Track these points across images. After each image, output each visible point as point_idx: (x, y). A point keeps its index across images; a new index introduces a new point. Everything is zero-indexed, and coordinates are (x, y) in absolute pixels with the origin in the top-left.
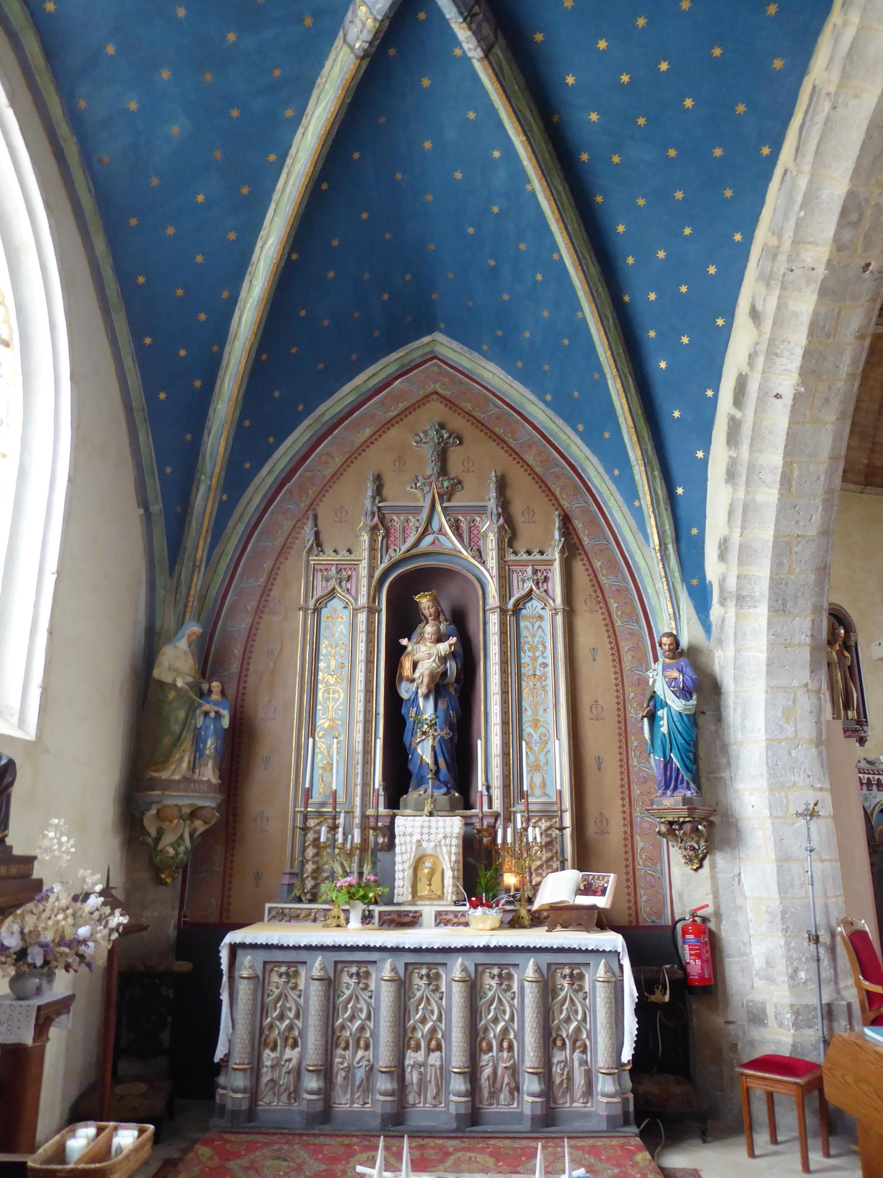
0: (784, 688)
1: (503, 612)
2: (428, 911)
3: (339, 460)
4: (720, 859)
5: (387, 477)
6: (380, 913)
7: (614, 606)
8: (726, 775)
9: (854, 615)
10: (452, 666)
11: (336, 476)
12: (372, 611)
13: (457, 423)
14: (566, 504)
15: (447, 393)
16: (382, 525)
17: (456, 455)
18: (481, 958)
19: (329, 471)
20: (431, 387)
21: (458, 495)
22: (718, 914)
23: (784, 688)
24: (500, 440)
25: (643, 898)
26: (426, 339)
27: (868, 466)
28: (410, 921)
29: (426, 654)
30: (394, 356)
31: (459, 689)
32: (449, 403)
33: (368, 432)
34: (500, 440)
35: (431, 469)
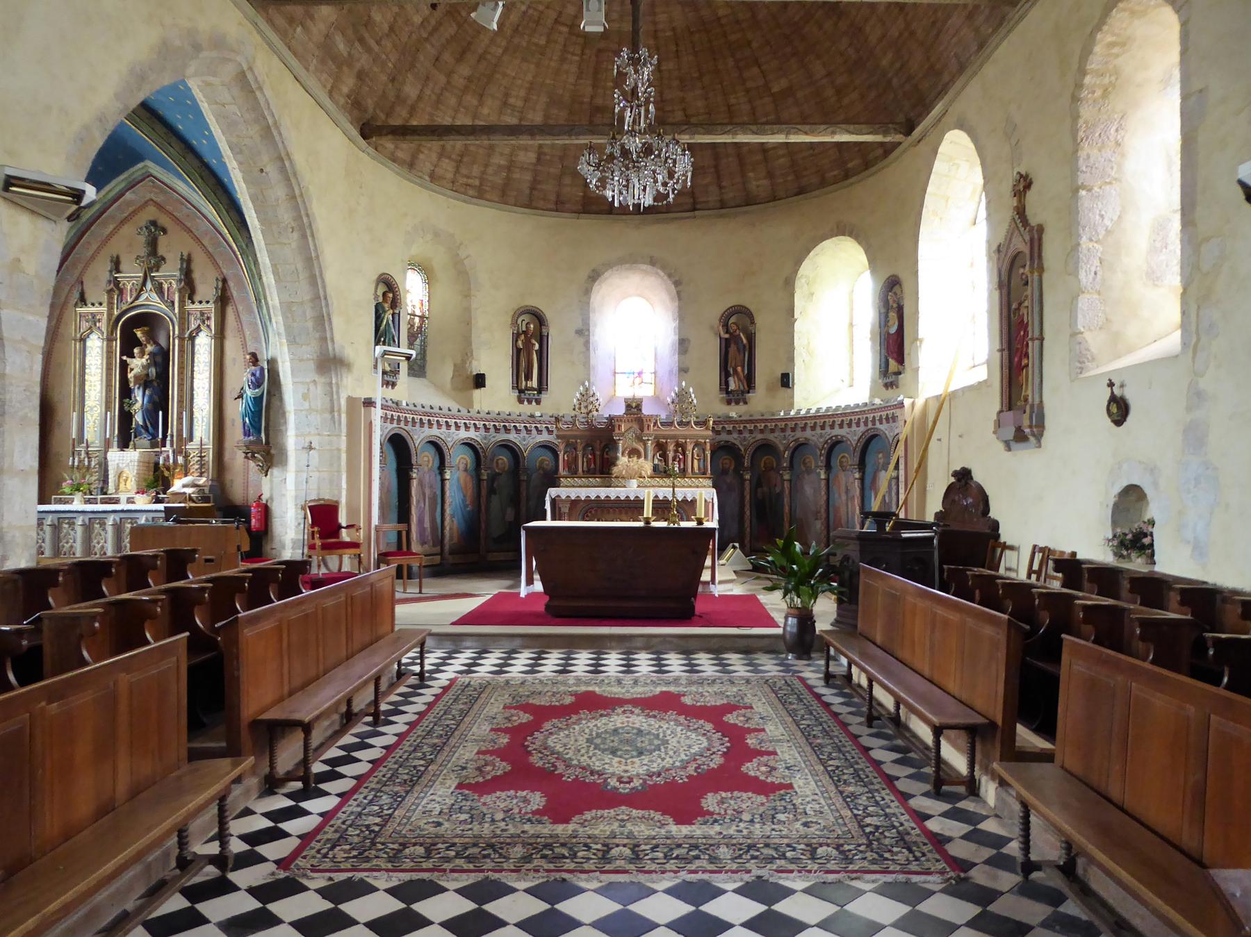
0: (302, 383)
1: (181, 339)
2: (123, 497)
3: (94, 247)
4: (275, 472)
5: (123, 259)
6: (544, 519)
7: (247, 333)
8: (283, 428)
9: (549, 314)
10: (153, 371)
11: (93, 258)
12: (110, 340)
13: (164, 221)
14: (225, 271)
15: (158, 200)
16: (116, 288)
17: (162, 241)
18: (122, 515)
19: (90, 253)
20: (148, 196)
21: (163, 267)
22: (271, 498)
23: (302, 383)
24: (189, 231)
25: (251, 491)
26: (140, 165)
27: (584, 197)
28: (117, 501)
29: (137, 364)
30: (122, 177)
31: (158, 385)
32: (159, 206)
33: (112, 227)
34: (189, 231)
35: (143, 251)
